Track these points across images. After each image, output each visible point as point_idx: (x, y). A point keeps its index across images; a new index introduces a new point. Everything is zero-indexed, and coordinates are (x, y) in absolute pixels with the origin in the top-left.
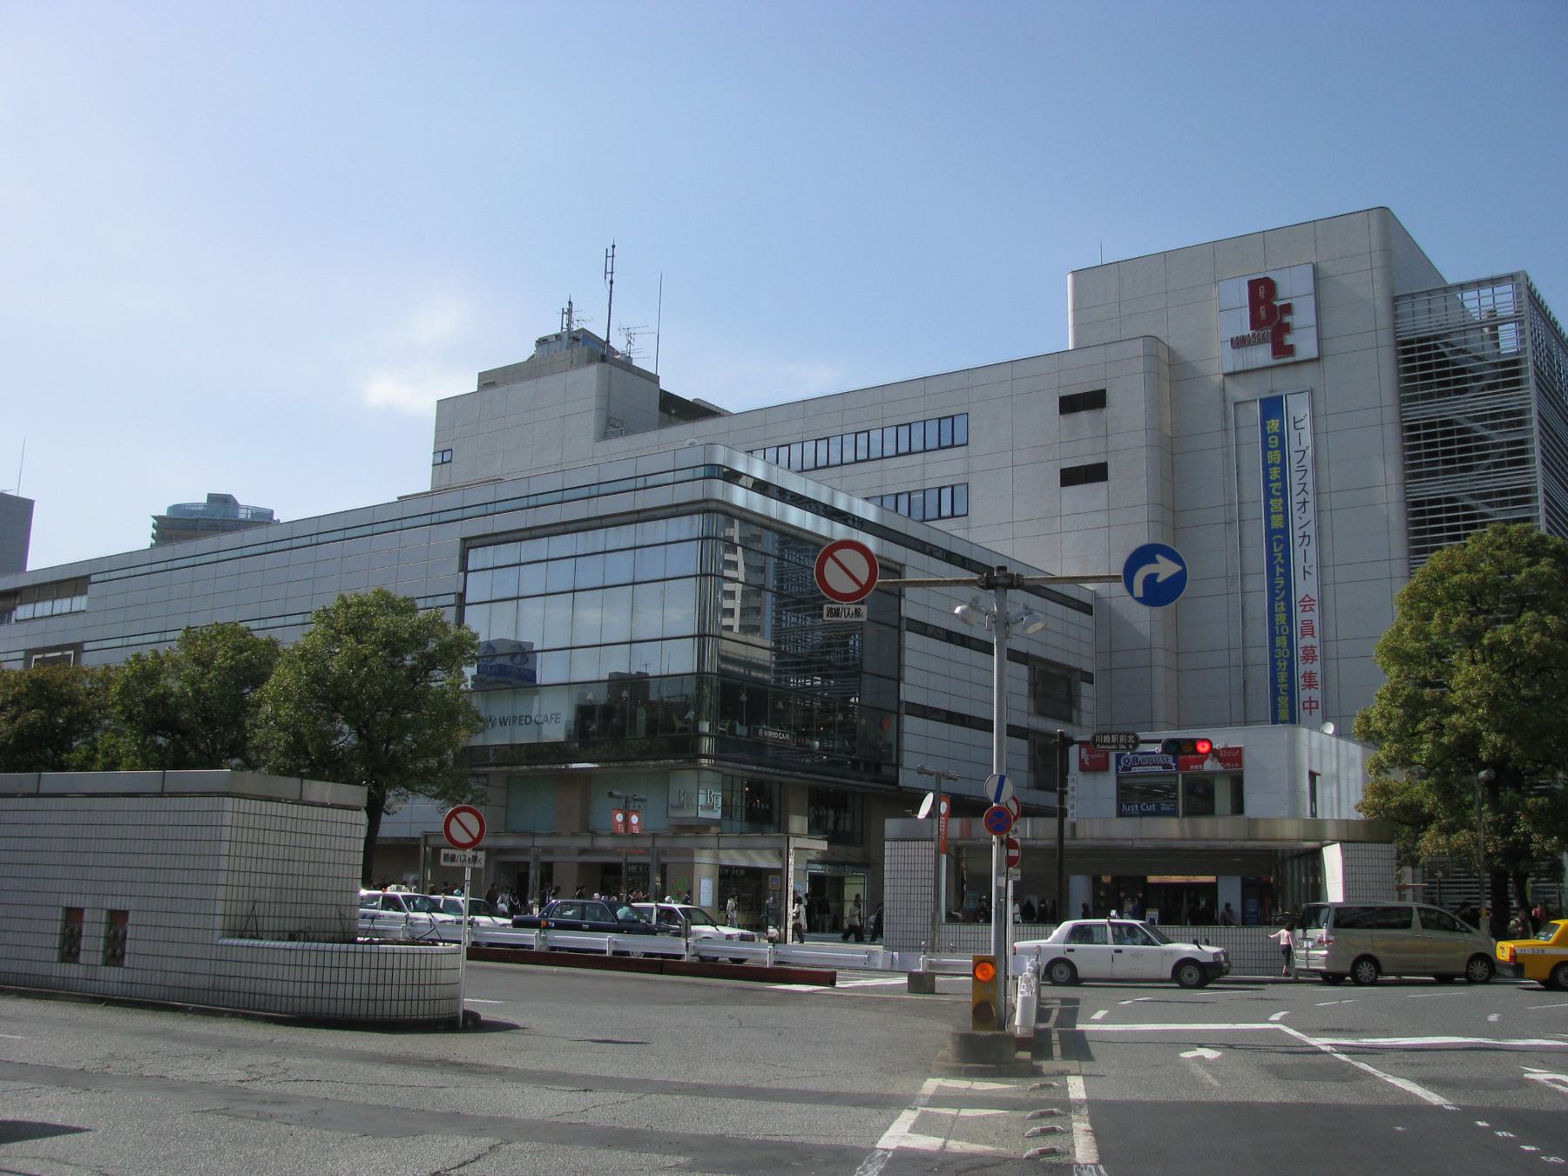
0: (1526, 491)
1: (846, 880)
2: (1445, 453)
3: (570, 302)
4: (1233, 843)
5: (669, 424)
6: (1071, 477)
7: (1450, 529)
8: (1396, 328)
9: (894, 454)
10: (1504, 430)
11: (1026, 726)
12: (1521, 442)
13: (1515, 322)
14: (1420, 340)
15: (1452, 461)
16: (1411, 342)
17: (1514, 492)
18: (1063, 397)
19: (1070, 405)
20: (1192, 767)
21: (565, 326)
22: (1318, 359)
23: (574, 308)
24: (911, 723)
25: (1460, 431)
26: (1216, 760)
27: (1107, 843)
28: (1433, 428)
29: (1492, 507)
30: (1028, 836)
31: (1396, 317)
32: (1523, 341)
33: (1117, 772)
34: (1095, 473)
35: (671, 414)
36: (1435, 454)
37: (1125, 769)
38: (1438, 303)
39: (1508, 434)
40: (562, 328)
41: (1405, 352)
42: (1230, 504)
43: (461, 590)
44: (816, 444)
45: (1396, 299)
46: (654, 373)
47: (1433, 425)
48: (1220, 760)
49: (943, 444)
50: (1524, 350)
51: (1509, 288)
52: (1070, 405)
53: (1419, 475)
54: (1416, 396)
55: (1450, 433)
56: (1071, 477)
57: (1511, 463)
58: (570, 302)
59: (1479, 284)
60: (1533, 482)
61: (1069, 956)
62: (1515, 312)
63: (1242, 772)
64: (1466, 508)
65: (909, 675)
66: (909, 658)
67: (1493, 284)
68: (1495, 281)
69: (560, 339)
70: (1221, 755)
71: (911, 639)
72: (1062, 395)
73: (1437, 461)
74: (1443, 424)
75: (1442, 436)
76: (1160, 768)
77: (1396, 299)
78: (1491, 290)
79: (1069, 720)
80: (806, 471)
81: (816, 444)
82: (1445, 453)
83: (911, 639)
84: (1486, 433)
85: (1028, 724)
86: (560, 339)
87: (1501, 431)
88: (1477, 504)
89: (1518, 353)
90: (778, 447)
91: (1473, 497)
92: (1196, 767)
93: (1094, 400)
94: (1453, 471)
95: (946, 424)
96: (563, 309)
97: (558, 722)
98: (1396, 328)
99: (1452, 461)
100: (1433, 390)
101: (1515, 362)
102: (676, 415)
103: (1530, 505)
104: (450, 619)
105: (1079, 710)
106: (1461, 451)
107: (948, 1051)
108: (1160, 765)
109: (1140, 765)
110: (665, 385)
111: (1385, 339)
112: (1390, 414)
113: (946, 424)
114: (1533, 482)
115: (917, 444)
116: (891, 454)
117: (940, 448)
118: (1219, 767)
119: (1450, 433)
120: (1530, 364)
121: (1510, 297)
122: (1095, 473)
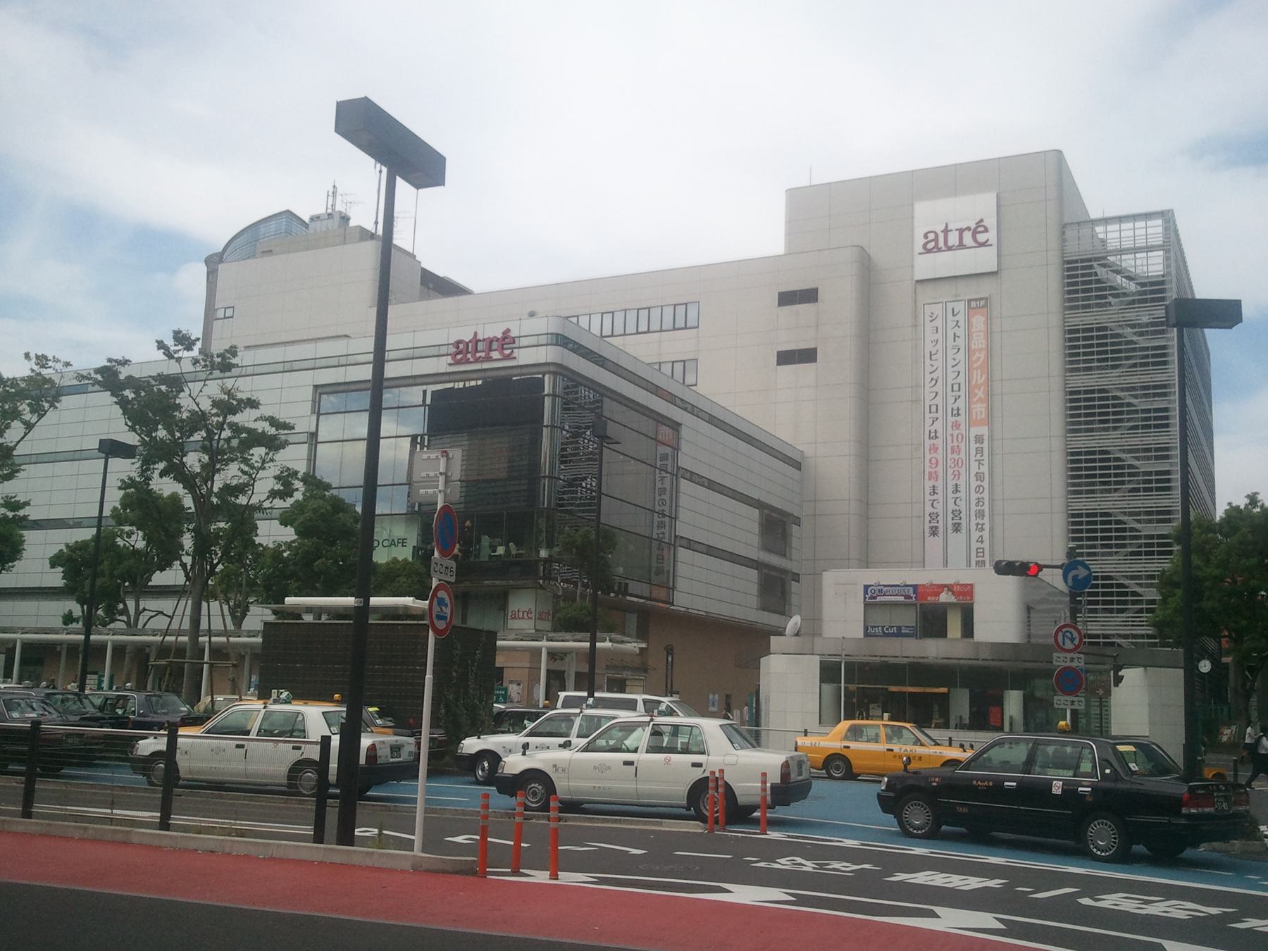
0: (1165, 386)
1: (628, 682)
2: (1099, 353)
3: (334, 186)
4: (854, 658)
5: (429, 298)
6: (785, 358)
7: (1100, 414)
8: (1064, 250)
9: (672, 328)
10: (1149, 337)
11: (756, 559)
12: (1164, 347)
13: (1163, 250)
14: (1083, 261)
15: (1106, 360)
16: (1076, 261)
17: (1155, 387)
18: (783, 293)
19: (787, 299)
20: (929, 598)
21: (330, 206)
22: (997, 272)
23: (339, 191)
24: (683, 553)
25: (1113, 336)
26: (950, 593)
27: (921, 661)
28: (1086, 336)
29: (1137, 399)
30: (598, 644)
31: (1064, 240)
32: (1168, 266)
33: (864, 600)
34: (808, 356)
35: (429, 288)
36: (1092, 353)
37: (871, 598)
38: (1085, 231)
39: (1152, 340)
40: (327, 209)
41: (1069, 269)
42: (917, 386)
43: (313, 429)
44: (638, 313)
45: (1064, 226)
46: (412, 252)
47: (1091, 330)
48: (953, 593)
49: (640, 330)
50: (1169, 273)
51: (1160, 222)
52: (787, 299)
53: (1078, 370)
54: (1078, 306)
55: (1105, 337)
56: (785, 358)
57: (1154, 364)
58: (334, 186)
59: (1120, 219)
60: (1173, 380)
61: (845, 752)
62: (1164, 242)
63: (973, 603)
64: (1115, 398)
65: (683, 514)
66: (684, 500)
67: (1147, 218)
68: (1147, 216)
69: (332, 218)
70: (955, 590)
71: (684, 484)
72: (780, 291)
73: (1093, 359)
74: (1099, 329)
75: (1097, 339)
76: (902, 599)
77: (1064, 226)
78: (1118, 225)
79: (784, 555)
80: (664, 331)
81: (638, 313)
82: (1099, 353)
83: (684, 484)
84: (1135, 338)
85: (758, 558)
86: (332, 218)
87: (1147, 337)
88: (1125, 395)
89: (1163, 276)
90: (602, 314)
91: (1122, 390)
92: (933, 598)
93: (809, 296)
94: (1106, 368)
95: (644, 313)
96: (328, 192)
97: (405, 546)
98: (1064, 250)
99: (1106, 360)
100: (1091, 302)
101: (1162, 283)
102: (434, 289)
103: (1168, 398)
104: (197, 458)
105: (791, 547)
106: (1113, 352)
107: (480, 806)
108: (902, 595)
109: (884, 595)
110: (423, 265)
111: (1054, 259)
112: (1055, 319)
113: (644, 313)
114: (1173, 380)
115: (655, 326)
116: (668, 328)
117: (674, 329)
118: (953, 599)
119: (1105, 337)
120: (1174, 285)
121: (1160, 230)
122: (808, 356)
